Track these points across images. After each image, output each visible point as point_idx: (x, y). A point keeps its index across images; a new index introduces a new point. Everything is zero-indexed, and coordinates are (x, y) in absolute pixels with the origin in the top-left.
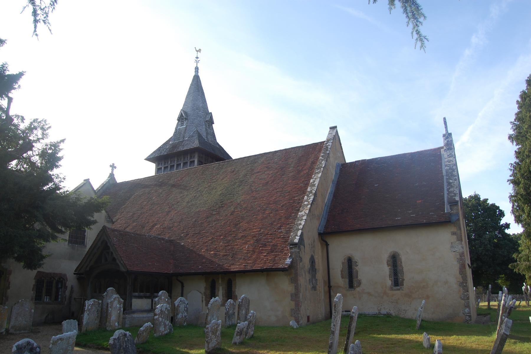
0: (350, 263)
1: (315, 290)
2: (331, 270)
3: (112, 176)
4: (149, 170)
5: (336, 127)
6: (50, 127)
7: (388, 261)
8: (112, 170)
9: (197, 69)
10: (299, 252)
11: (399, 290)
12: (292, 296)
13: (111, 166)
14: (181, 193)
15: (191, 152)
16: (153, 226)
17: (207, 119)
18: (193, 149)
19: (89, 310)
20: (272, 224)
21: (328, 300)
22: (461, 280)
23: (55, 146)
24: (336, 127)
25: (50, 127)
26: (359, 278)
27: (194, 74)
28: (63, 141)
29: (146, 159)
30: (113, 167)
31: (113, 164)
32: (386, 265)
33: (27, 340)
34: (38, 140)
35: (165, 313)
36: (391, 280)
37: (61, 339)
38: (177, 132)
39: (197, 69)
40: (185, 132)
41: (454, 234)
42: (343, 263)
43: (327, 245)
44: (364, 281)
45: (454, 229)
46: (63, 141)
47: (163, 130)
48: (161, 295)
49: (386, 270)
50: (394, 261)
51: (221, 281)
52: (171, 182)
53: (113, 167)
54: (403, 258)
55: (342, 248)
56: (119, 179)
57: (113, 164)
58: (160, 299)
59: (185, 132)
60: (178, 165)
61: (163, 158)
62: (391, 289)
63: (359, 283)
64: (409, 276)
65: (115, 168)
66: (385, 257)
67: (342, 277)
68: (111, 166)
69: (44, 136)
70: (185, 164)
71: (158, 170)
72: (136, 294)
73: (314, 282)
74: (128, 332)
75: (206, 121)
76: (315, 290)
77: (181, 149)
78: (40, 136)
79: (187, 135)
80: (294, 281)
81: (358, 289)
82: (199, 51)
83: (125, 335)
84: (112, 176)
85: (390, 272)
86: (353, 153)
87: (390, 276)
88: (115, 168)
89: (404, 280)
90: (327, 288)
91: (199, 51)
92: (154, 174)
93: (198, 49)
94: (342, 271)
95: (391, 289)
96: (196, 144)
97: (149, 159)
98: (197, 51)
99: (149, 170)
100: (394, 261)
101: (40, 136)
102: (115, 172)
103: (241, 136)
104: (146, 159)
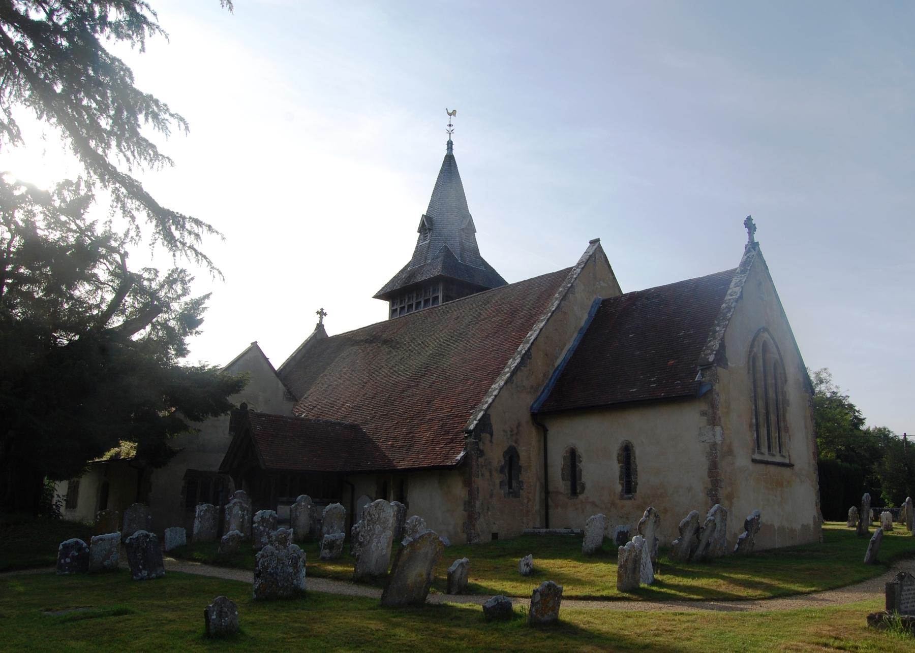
0: (573, 457)
1: (516, 495)
2: (550, 470)
3: (320, 327)
4: (381, 312)
5: (598, 240)
6: (192, 279)
7: (619, 455)
8: (321, 318)
9: (450, 144)
10: (477, 444)
11: (630, 499)
12: (465, 504)
13: (318, 313)
14: (389, 353)
15: (433, 282)
16: (343, 405)
17: (464, 226)
18: (442, 277)
19: (201, 517)
20: (467, 401)
21: (543, 513)
22: (710, 486)
23: (197, 305)
24: (598, 240)
25: (192, 279)
26: (583, 480)
27: (445, 153)
28: (207, 296)
29: (595, 242)
30: (322, 313)
31: (322, 309)
32: (616, 462)
33: (75, 539)
34: (179, 297)
35: (269, 520)
36: (622, 484)
37: (101, 539)
38: (419, 253)
39: (450, 144)
40: (427, 252)
41: (704, 414)
42: (565, 458)
43: (545, 431)
44: (588, 486)
45: (704, 407)
46: (207, 296)
47: (398, 251)
48: (300, 501)
49: (616, 468)
50: (627, 455)
51: (395, 482)
52: (384, 336)
53: (322, 313)
54: (638, 451)
55: (568, 434)
56: (332, 331)
57: (322, 309)
58: (299, 504)
59: (427, 252)
60: (418, 304)
61: (398, 293)
62: (622, 498)
63: (583, 488)
64: (644, 479)
65: (325, 314)
66: (615, 449)
67: (563, 479)
68: (318, 313)
69: (185, 292)
70: (427, 301)
71: (393, 312)
72: (285, 499)
73: (514, 484)
74: (151, 534)
75: (463, 230)
76: (516, 495)
77: (420, 278)
78: (180, 292)
79: (430, 255)
80: (468, 483)
81: (581, 497)
82: (454, 113)
83: (148, 536)
84: (320, 327)
85: (621, 472)
86: (632, 279)
87: (621, 478)
88: (325, 314)
89: (637, 484)
90: (543, 495)
91: (454, 113)
92: (387, 318)
93: (450, 111)
94: (563, 470)
95: (622, 498)
96: (437, 270)
97: (381, 296)
98: (450, 114)
99: (381, 312)
100: (627, 455)
101: (180, 292)
102: (326, 321)
103: (517, 249)
104: (595, 242)
